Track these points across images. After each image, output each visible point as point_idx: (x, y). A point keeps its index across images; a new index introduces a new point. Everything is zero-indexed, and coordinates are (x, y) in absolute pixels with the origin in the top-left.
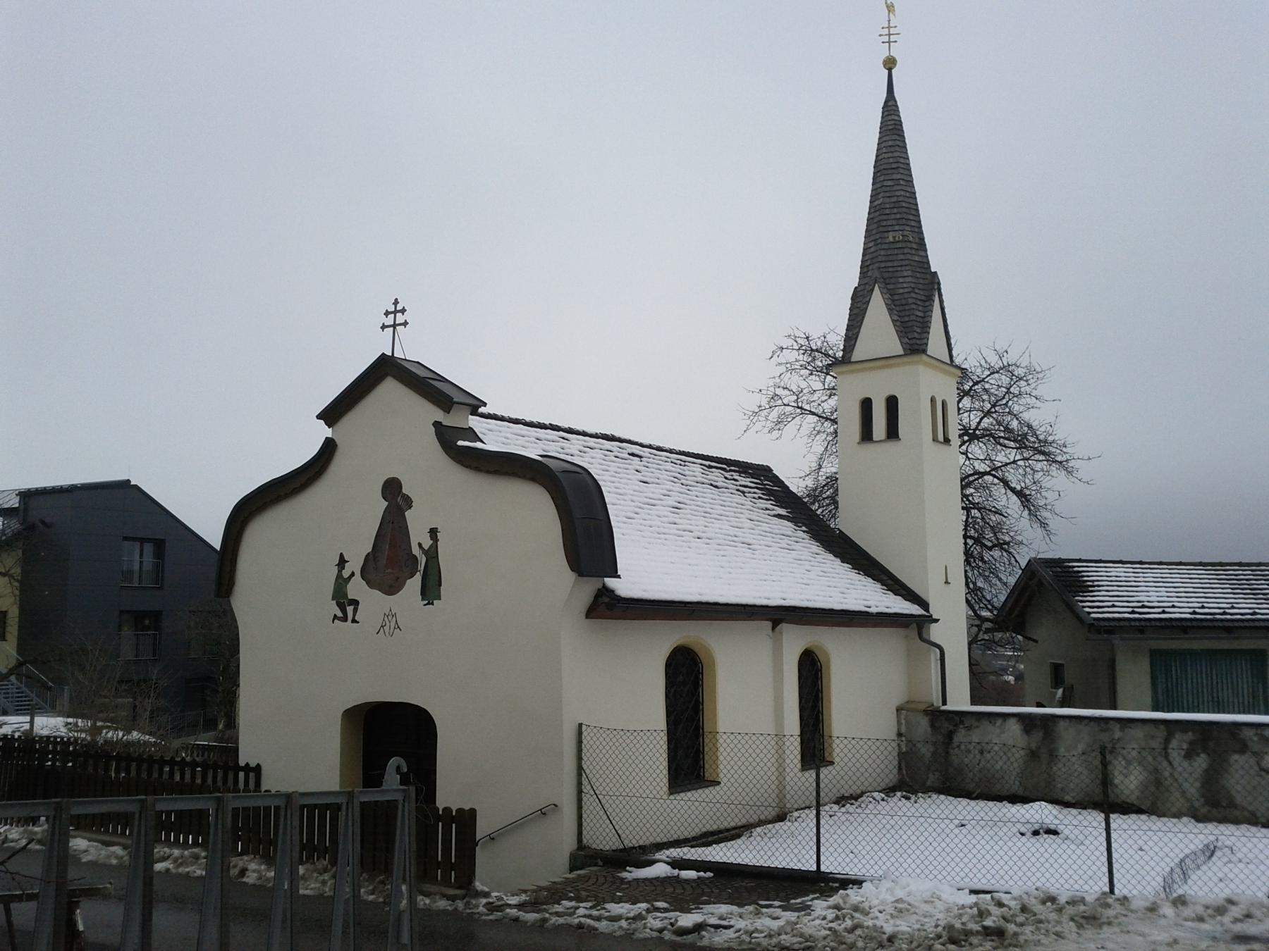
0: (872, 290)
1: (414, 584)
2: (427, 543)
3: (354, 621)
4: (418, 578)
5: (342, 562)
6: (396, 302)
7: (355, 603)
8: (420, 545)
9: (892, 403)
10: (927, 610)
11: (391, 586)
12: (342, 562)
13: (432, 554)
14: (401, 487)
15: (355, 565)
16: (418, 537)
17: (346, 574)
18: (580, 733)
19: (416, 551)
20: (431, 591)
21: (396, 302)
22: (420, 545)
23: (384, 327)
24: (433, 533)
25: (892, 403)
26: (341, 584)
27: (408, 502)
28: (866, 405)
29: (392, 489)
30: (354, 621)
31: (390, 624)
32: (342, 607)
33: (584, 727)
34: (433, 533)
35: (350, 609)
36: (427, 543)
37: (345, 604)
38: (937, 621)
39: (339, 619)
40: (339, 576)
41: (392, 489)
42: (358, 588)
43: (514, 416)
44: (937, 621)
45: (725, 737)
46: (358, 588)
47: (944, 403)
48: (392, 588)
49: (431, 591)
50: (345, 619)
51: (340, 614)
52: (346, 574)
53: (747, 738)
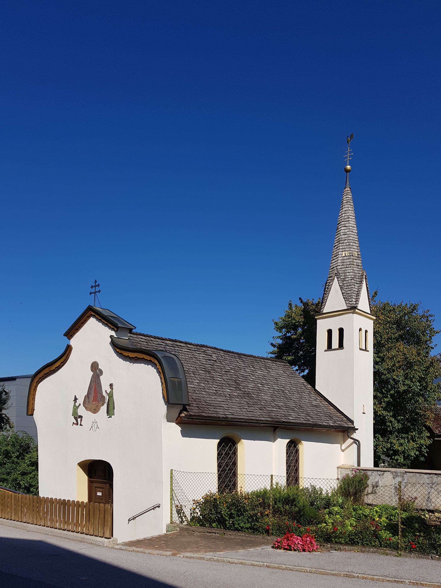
0: (334, 279)
1: (104, 408)
2: (109, 390)
3: (81, 425)
4: (105, 405)
5: (76, 399)
6: (96, 282)
7: (81, 417)
8: (106, 391)
9: (341, 331)
10: (353, 425)
11: (95, 409)
12: (76, 399)
13: (111, 395)
14: (98, 366)
15: (80, 401)
16: (105, 388)
17: (77, 404)
18: (172, 474)
19: (104, 394)
20: (110, 412)
21: (96, 282)
22: (106, 391)
23: (91, 293)
24: (111, 385)
25: (341, 331)
26: (76, 408)
27: (101, 372)
28: (330, 332)
29: (95, 367)
30: (81, 425)
31: (95, 426)
32: (76, 419)
33: (173, 471)
34: (111, 385)
35: (79, 420)
36: (109, 390)
37: (77, 417)
38: (357, 429)
39: (75, 424)
40: (75, 405)
41: (95, 367)
42: (82, 411)
43: (145, 333)
44: (357, 429)
45: (241, 476)
46: (82, 411)
47: (366, 331)
48: (95, 411)
49: (110, 412)
50: (77, 424)
51: (75, 422)
52: (77, 404)
53: (264, 477)
